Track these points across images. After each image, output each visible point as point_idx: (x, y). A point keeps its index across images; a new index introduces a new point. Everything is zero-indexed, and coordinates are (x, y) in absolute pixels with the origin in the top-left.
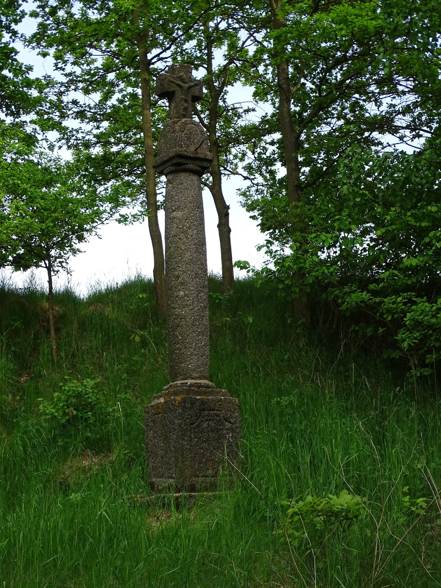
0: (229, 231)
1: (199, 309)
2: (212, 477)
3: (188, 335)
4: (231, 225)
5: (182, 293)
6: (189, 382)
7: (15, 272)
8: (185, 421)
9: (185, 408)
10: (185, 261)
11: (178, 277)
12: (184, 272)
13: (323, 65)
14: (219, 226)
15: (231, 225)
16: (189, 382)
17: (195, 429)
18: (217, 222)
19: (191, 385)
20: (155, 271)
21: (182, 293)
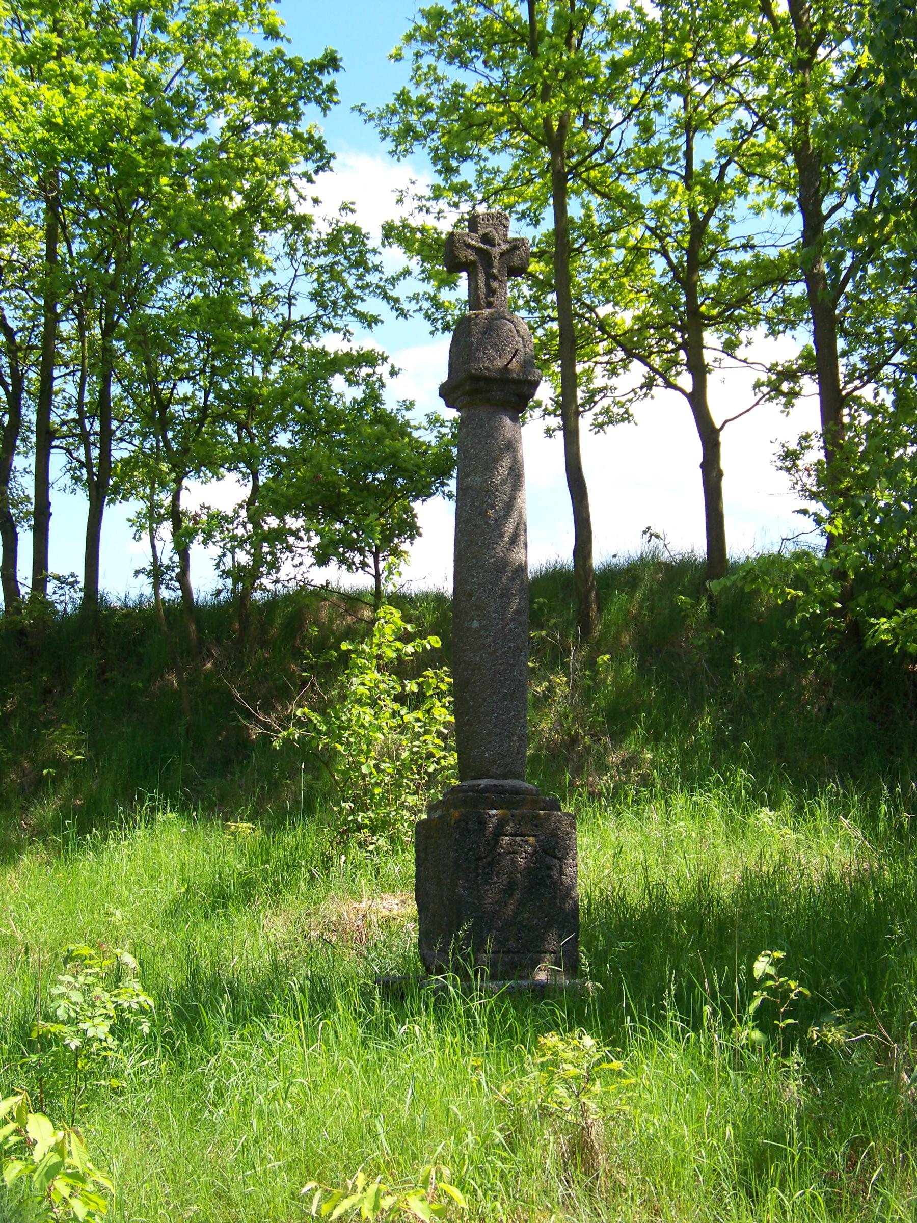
0: (720, 474)
1: (505, 653)
2: (515, 953)
3: (484, 699)
4: (724, 464)
5: (476, 624)
6: (484, 782)
7: (316, 567)
8: (467, 854)
9: (467, 830)
10: (482, 566)
11: (470, 595)
12: (481, 585)
13: (95, 145)
14: (702, 466)
15: (723, 466)
16: (484, 782)
17: (485, 868)
18: (700, 459)
19: (487, 789)
20: (575, 552)
21: (476, 624)
